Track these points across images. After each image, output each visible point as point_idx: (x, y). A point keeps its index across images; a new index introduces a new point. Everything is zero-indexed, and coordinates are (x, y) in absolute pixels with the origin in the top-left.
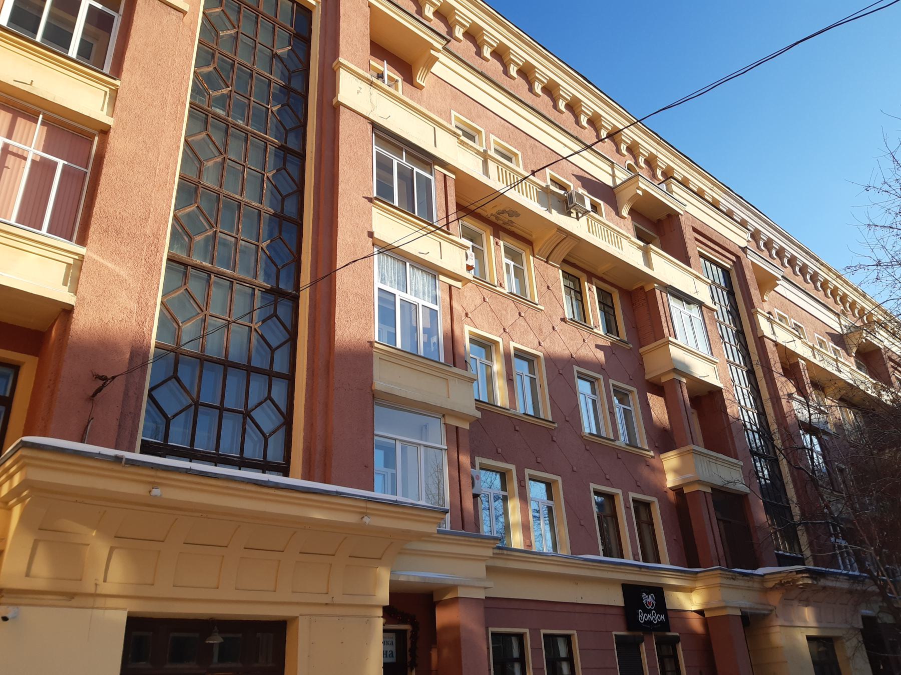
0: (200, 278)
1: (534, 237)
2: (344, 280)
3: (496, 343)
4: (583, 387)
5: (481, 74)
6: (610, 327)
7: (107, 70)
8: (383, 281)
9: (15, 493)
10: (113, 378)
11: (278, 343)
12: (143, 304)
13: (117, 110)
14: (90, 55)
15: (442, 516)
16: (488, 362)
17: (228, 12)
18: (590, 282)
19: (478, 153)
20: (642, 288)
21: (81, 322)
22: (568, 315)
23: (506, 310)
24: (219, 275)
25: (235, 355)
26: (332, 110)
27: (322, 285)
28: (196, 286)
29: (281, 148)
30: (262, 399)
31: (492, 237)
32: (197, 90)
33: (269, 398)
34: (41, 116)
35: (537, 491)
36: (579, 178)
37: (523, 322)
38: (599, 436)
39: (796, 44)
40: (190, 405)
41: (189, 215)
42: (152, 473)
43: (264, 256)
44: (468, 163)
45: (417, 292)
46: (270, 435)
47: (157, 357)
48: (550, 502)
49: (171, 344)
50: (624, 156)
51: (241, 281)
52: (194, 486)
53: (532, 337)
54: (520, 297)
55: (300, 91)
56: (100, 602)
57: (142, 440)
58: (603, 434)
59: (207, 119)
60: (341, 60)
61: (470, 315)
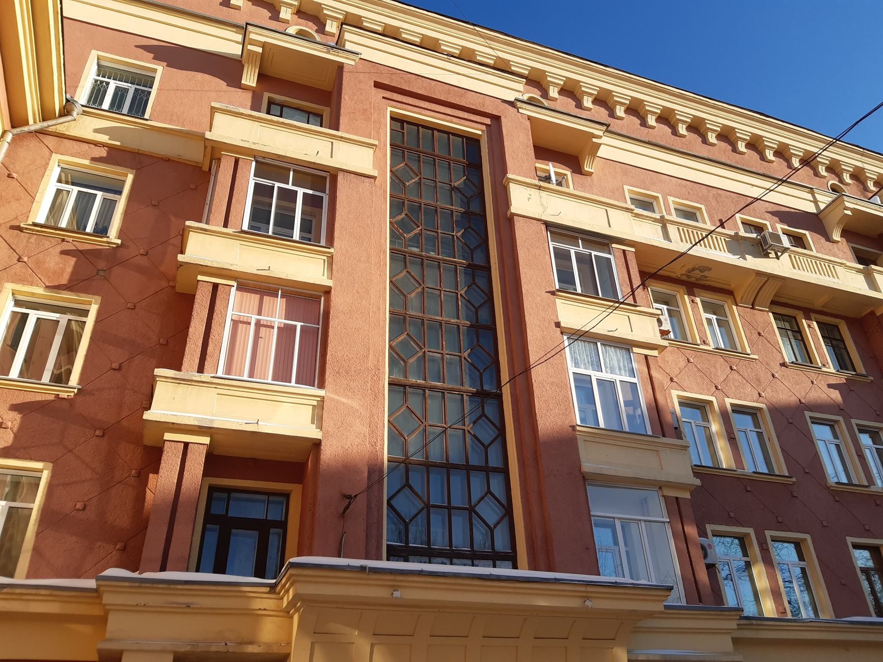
1: (733, 286)
2: (538, 375)
3: (710, 403)
4: (821, 433)
5: (649, 143)
6: (843, 361)
7: (323, 242)
8: (577, 365)
9: (292, 604)
10: (356, 496)
13: (335, 272)
14: (310, 233)
15: (667, 593)
16: (705, 424)
17: (410, 165)
18: (808, 318)
19: (655, 220)
20: (872, 313)
21: (328, 453)
22: (788, 357)
23: (715, 367)
24: (432, 388)
25: (455, 457)
26: (507, 221)
27: (520, 380)
28: (414, 402)
29: (469, 266)
30: (483, 494)
31: (686, 297)
32: (394, 237)
33: (489, 492)
34: (291, 173)
35: (786, 553)
36: (774, 213)
37: (736, 376)
38: (850, 484)
39: (855, 124)
40: (423, 509)
41: (402, 342)
42: (392, 577)
43: (467, 364)
44: (644, 232)
45: (613, 370)
46: (495, 527)
47: (391, 470)
48: (802, 563)
49: (401, 457)
50: (824, 177)
51: (450, 390)
52: (428, 586)
53: (749, 389)
54: (731, 349)
55: (478, 212)
57: (387, 545)
58: (855, 481)
59: (405, 258)
60: (509, 176)
61: (675, 379)
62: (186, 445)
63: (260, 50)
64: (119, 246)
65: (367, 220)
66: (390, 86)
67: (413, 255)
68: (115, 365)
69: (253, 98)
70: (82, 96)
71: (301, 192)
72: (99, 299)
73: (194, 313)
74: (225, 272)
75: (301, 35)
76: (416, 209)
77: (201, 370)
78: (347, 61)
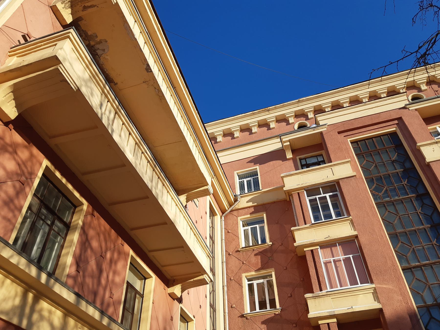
0: (418, 270)
11: (431, 212)
12: (404, 295)
13: (356, 227)
21: (388, 313)
24: (425, 265)
28: (418, 274)
29: (417, 196)
51: (434, 263)
62: (328, 324)
63: (288, 143)
64: (272, 245)
65: (362, 197)
66: (345, 130)
67: (387, 202)
68: (289, 295)
69: (293, 162)
70: (238, 192)
71: (327, 195)
72: (273, 269)
73: (309, 266)
74: (313, 244)
75: (302, 127)
76: (379, 179)
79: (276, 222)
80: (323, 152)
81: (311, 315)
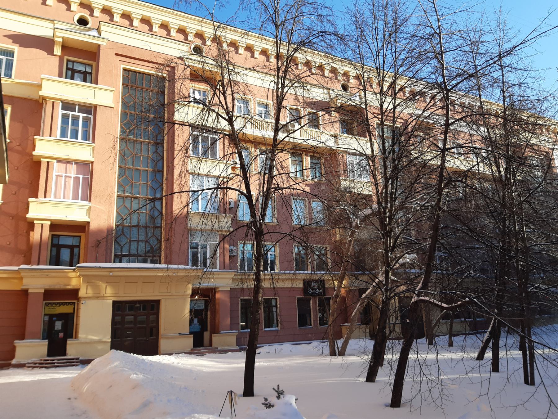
14: (86, 137)
21: (93, 226)
34: (77, 107)
47: (116, 230)
56: (105, 298)
62: (42, 224)
65: (110, 125)
68: (13, 192)
77: (45, 197)
78: (102, 43)
79: (21, 121)
80: (94, 64)
81: (28, 216)
